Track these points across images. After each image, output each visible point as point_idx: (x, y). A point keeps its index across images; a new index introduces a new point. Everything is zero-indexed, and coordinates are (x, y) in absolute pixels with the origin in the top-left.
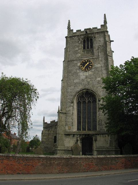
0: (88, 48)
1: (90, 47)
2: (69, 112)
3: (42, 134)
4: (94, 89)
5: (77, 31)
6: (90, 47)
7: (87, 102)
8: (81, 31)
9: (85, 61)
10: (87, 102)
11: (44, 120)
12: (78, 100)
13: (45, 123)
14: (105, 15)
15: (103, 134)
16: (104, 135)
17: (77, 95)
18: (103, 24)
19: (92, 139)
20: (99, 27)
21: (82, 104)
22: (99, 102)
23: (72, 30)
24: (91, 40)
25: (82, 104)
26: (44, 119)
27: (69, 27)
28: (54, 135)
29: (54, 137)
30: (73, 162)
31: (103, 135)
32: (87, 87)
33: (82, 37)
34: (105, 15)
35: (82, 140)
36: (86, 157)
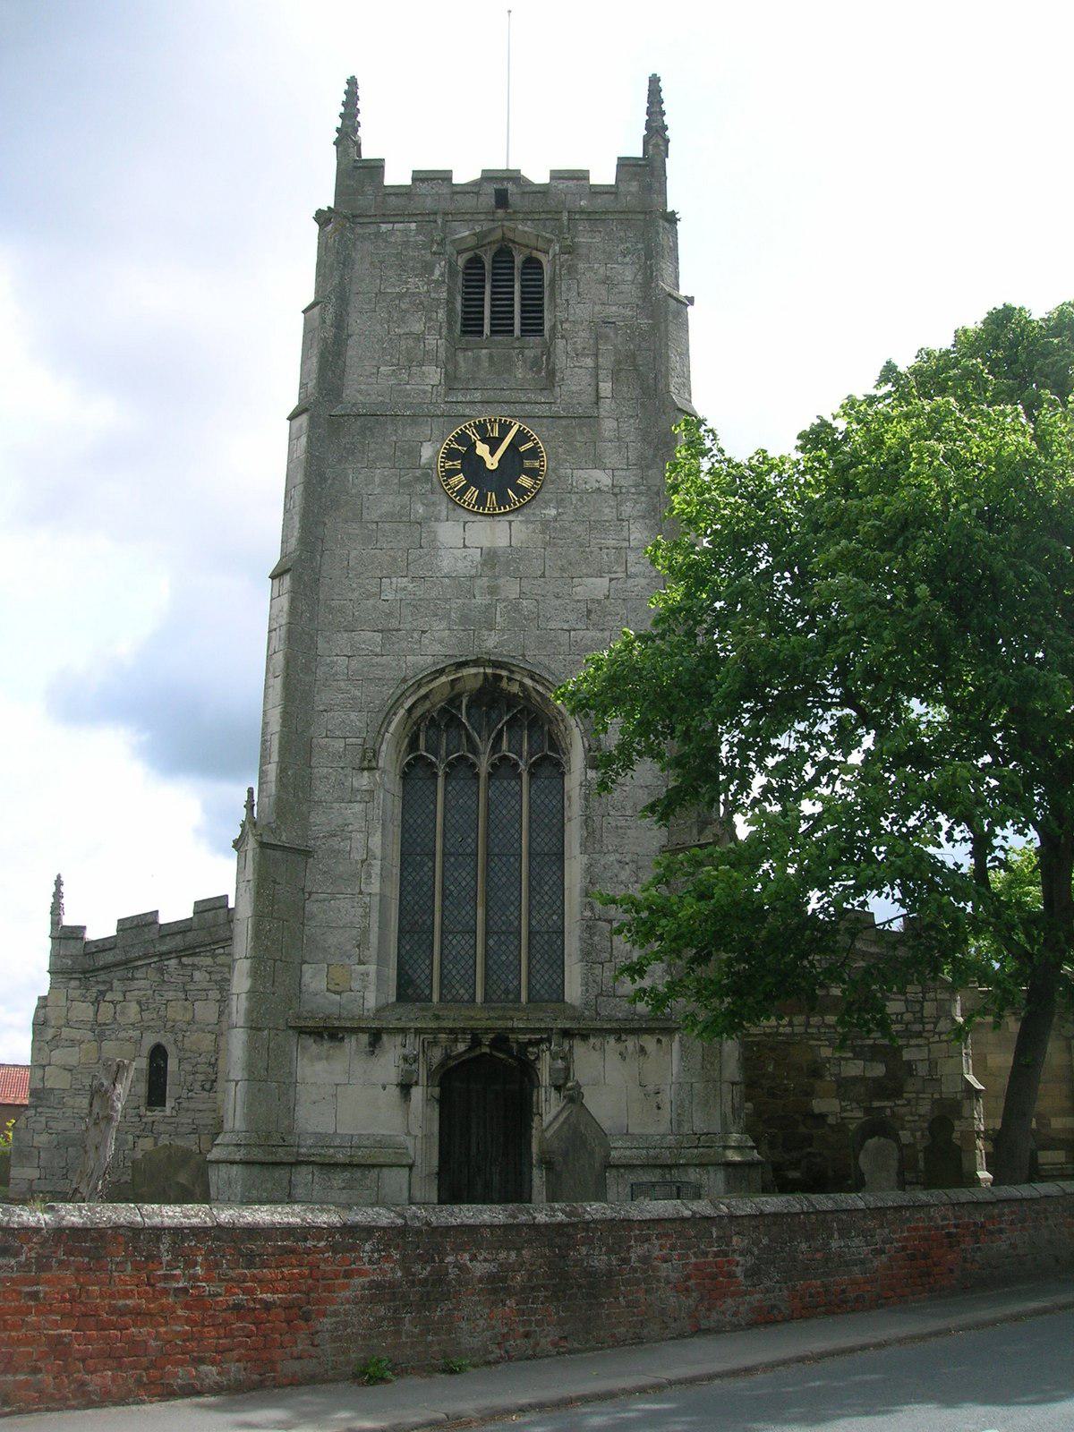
2: (335, 843)
3: (40, 1025)
5: (419, 177)
7: (484, 766)
8: (587, 179)
10: (484, 766)
11: (56, 909)
12: (413, 745)
13: (65, 936)
14: (654, 82)
15: (620, 1033)
16: (631, 1043)
17: (410, 710)
18: (637, 152)
19: (527, 1071)
20: (603, 175)
21: (441, 781)
23: (377, 167)
25: (441, 781)
26: (58, 895)
27: (347, 136)
28: (150, 1040)
29: (146, 1050)
30: (600, 1261)
31: (619, 1040)
34: (654, 82)
35: (440, 1085)
36: (687, 1213)
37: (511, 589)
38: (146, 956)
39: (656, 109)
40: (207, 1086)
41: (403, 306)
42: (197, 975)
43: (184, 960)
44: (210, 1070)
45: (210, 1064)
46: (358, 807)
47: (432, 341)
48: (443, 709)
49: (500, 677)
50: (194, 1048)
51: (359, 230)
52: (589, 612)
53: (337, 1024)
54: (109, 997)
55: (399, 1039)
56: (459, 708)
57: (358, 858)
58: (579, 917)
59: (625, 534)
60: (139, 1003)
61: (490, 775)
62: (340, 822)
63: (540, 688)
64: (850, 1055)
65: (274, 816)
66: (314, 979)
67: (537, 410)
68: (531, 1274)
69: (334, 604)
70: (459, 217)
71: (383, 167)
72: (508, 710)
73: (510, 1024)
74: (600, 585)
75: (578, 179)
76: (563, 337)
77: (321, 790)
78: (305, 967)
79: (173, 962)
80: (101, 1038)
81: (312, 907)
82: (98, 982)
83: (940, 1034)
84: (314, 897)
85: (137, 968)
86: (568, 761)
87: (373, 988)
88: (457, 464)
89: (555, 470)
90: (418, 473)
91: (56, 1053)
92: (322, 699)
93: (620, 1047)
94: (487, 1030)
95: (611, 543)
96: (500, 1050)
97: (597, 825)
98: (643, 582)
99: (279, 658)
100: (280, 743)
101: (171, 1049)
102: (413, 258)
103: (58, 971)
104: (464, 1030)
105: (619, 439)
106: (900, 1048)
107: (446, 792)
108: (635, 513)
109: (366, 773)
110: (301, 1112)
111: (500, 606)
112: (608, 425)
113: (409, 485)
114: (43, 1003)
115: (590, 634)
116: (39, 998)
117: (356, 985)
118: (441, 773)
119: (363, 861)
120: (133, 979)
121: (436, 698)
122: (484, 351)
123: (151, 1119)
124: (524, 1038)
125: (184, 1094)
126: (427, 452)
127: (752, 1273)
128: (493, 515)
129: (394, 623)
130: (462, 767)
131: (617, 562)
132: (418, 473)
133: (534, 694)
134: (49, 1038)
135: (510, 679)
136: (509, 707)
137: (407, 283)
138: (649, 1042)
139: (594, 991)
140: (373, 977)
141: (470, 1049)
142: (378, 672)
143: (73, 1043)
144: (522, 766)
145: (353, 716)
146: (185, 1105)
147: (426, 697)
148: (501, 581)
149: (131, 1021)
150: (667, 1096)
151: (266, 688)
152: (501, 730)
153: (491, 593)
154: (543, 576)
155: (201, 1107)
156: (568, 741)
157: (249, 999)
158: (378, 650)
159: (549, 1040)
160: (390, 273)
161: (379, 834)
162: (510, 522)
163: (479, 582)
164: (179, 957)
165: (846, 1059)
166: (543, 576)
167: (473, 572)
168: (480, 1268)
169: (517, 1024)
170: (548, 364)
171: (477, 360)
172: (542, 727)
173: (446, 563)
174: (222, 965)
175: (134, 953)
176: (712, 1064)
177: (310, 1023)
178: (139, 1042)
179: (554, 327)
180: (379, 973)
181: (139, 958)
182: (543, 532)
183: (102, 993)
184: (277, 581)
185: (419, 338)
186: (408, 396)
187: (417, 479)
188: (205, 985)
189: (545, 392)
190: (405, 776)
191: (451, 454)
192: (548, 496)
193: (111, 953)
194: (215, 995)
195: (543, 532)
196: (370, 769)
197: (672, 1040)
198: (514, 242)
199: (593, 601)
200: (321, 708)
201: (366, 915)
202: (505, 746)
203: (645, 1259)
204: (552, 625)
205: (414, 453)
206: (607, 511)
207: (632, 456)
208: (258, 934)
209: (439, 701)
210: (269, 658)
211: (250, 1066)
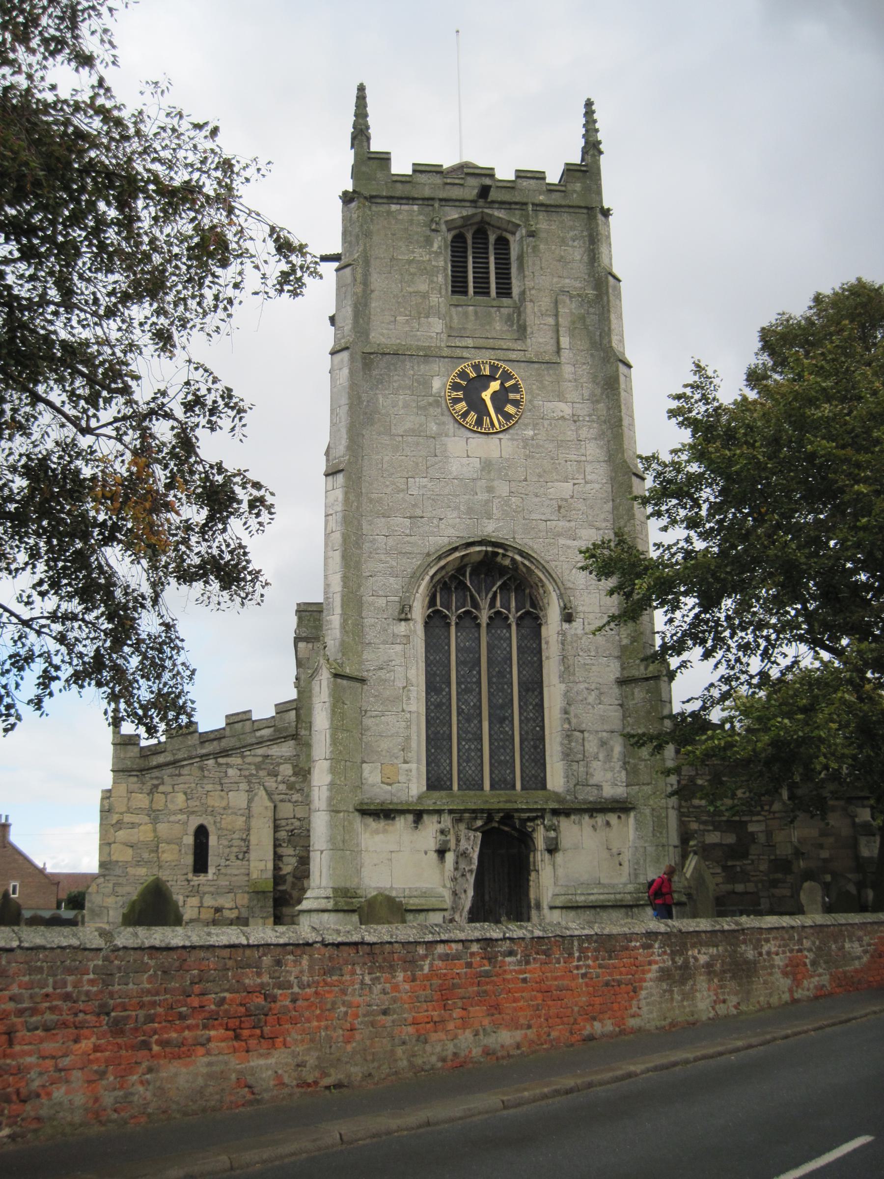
0: (482, 289)
1: (493, 286)
3: (106, 812)
4: (536, 546)
6: (493, 286)
7: (484, 619)
8: (544, 179)
9: (476, 367)
10: (484, 619)
16: (600, 819)
17: (432, 577)
18: (576, 159)
20: (553, 177)
21: (453, 629)
22: (566, 626)
23: (384, 159)
24: (503, 244)
25: (453, 629)
28: (195, 822)
29: (192, 829)
31: (591, 816)
32: (490, 529)
33: (454, 214)
34: (361, 89)
37: (502, 488)
38: (191, 758)
39: (590, 127)
40: (241, 856)
41: (412, 270)
42: (231, 772)
43: (221, 760)
44: (242, 844)
45: (242, 839)
46: (398, 648)
47: (434, 299)
48: (453, 575)
49: (497, 554)
50: (230, 827)
51: (374, 208)
52: (560, 507)
53: (391, 807)
54: (161, 788)
55: (435, 818)
56: (464, 575)
57: (401, 686)
58: (559, 729)
59: (583, 451)
60: (185, 793)
61: (488, 625)
62: (386, 659)
63: (527, 563)
64: (711, 828)
65: (340, 655)
66: (372, 775)
67: (513, 356)
68: (723, 963)
69: (373, 496)
70: (451, 204)
71: (389, 159)
72: (500, 578)
73: (516, 806)
74: (566, 489)
75: (538, 178)
76: (531, 301)
77: (370, 635)
78: (364, 765)
79: (211, 762)
80: (155, 821)
81: (367, 721)
82: (152, 778)
83: (774, 813)
84: (369, 714)
85: (183, 766)
86: (545, 616)
87: (414, 780)
88: (460, 394)
89: (531, 401)
90: (431, 399)
91: (121, 833)
92: (368, 567)
93: (592, 821)
94: (499, 811)
95: (574, 457)
96: (506, 825)
97: (571, 662)
98: (597, 486)
99: (337, 537)
100: (342, 600)
101: (211, 829)
102: (417, 233)
103: (119, 771)
104: (482, 811)
105: (575, 380)
106: (746, 823)
107: (457, 637)
108: (589, 436)
109: (403, 623)
110: (365, 872)
111: (496, 501)
112: (567, 370)
113: (424, 408)
114: (107, 795)
115: (561, 524)
116: (103, 791)
117: (402, 778)
118: (453, 623)
119: (404, 688)
120: (180, 775)
121: (449, 568)
122: (471, 308)
123: (196, 883)
124: (525, 815)
125: (223, 862)
126: (437, 384)
127: (814, 963)
128: (487, 434)
129: (418, 512)
130: (469, 619)
131: (578, 472)
132: (431, 399)
133: (521, 567)
134: (114, 822)
135: (504, 555)
136: (501, 575)
137: (413, 252)
138: (613, 818)
139: (573, 782)
140: (414, 772)
141: (486, 824)
142: (408, 549)
143: (133, 825)
144: (512, 620)
145: (392, 580)
146: (223, 871)
147: (443, 568)
148: (496, 483)
149: (180, 807)
150: (627, 856)
151: (326, 558)
152: (495, 592)
153: (489, 492)
154: (525, 480)
155: (236, 872)
156: (545, 601)
157: (330, 790)
158: (408, 532)
159: (543, 817)
160: (400, 244)
161: (414, 667)
162: (500, 439)
163: (479, 483)
164: (216, 758)
165: (708, 831)
166: (525, 480)
167: (475, 476)
168: (703, 959)
169: (520, 806)
170: (518, 320)
171: (466, 314)
172: (524, 590)
173: (455, 467)
174: (249, 764)
175: (180, 756)
176: (661, 833)
177: (372, 807)
178: (186, 823)
179: (523, 293)
180: (418, 769)
181: (185, 759)
182: (524, 448)
183: (156, 786)
184: (330, 478)
185: (425, 296)
186: (419, 340)
187: (430, 404)
188: (237, 779)
189: (519, 342)
190: (427, 624)
191: (455, 387)
192: (527, 421)
193: (163, 755)
194: (244, 786)
195: (524, 448)
196: (406, 620)
197: (628, 816)
198: (489, 224)
199: (562, 499)
200: (368, 574)
201: (408, 727)
202: (498, 604)
203: (769, 953)
204: (534, 516)
205: (426, 384)
206: (569, 433)
207: (586, 394)
208: (334, 742)
209: (450, 570)
210: (327, 536)
211: (332, 839)
